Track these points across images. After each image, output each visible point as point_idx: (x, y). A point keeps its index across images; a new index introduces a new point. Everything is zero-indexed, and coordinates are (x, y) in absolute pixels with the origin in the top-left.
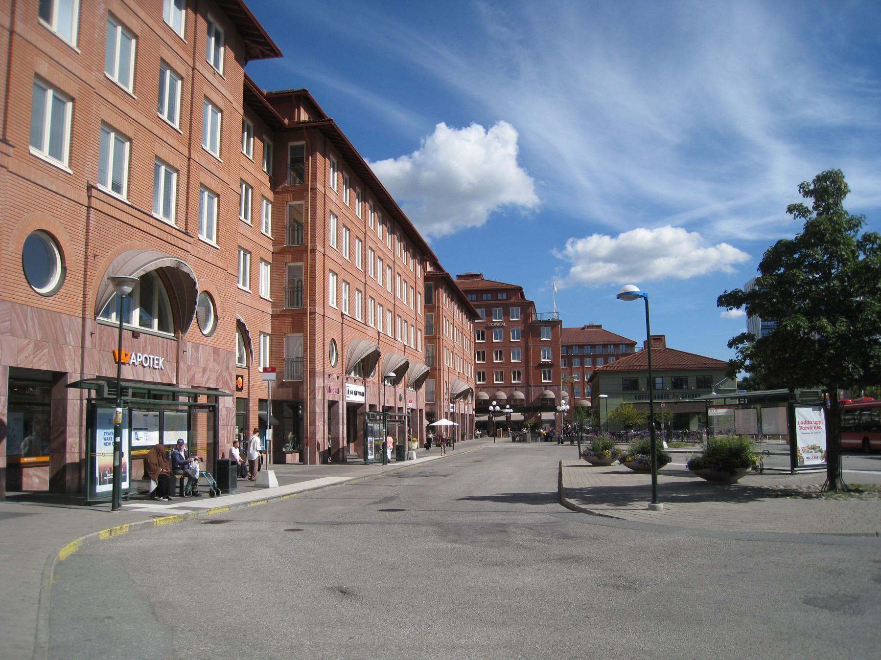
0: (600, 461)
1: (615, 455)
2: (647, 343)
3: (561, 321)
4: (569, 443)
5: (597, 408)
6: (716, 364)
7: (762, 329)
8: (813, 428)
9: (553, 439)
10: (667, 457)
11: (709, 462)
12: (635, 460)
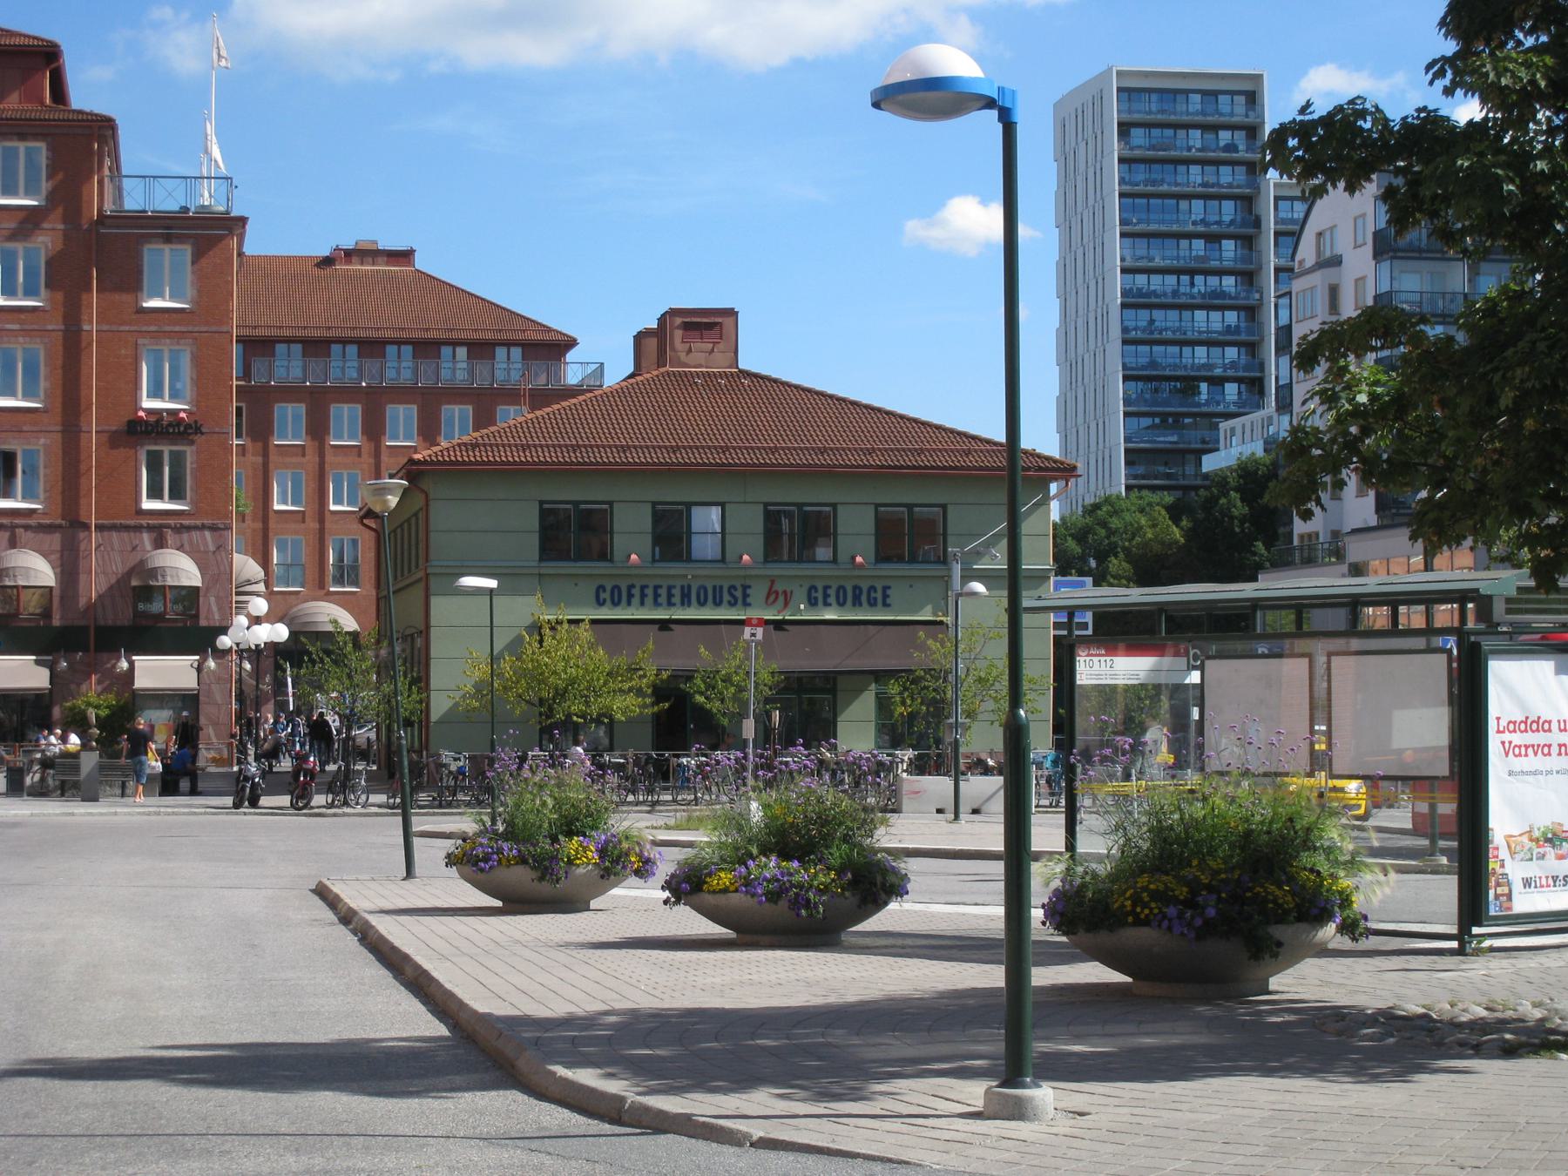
0: (545, 888)
1: (616, 861)
2: (652, 344)
3: (243, 221)
4: (285, 800)
5: (409, 638)
6: (968, 453)
7: (1124, 306)
8: (1555, 750)
9: (201, 785)
10: (895, 871)
11: (1156, 896)
12: (748, 883)
